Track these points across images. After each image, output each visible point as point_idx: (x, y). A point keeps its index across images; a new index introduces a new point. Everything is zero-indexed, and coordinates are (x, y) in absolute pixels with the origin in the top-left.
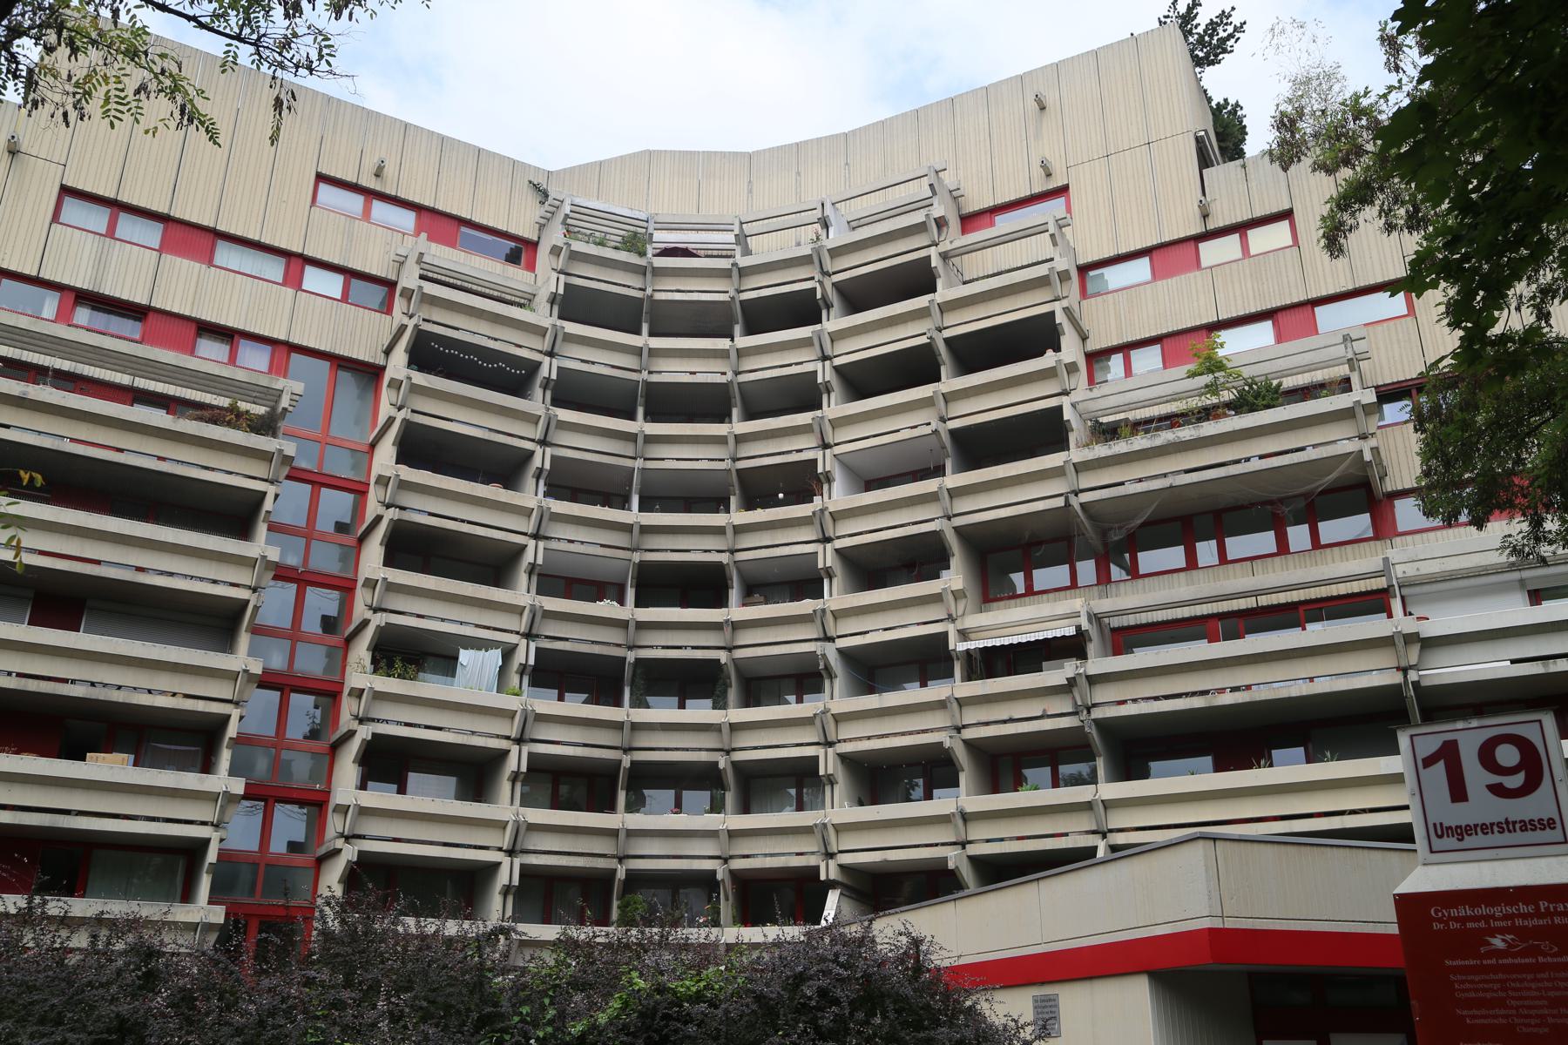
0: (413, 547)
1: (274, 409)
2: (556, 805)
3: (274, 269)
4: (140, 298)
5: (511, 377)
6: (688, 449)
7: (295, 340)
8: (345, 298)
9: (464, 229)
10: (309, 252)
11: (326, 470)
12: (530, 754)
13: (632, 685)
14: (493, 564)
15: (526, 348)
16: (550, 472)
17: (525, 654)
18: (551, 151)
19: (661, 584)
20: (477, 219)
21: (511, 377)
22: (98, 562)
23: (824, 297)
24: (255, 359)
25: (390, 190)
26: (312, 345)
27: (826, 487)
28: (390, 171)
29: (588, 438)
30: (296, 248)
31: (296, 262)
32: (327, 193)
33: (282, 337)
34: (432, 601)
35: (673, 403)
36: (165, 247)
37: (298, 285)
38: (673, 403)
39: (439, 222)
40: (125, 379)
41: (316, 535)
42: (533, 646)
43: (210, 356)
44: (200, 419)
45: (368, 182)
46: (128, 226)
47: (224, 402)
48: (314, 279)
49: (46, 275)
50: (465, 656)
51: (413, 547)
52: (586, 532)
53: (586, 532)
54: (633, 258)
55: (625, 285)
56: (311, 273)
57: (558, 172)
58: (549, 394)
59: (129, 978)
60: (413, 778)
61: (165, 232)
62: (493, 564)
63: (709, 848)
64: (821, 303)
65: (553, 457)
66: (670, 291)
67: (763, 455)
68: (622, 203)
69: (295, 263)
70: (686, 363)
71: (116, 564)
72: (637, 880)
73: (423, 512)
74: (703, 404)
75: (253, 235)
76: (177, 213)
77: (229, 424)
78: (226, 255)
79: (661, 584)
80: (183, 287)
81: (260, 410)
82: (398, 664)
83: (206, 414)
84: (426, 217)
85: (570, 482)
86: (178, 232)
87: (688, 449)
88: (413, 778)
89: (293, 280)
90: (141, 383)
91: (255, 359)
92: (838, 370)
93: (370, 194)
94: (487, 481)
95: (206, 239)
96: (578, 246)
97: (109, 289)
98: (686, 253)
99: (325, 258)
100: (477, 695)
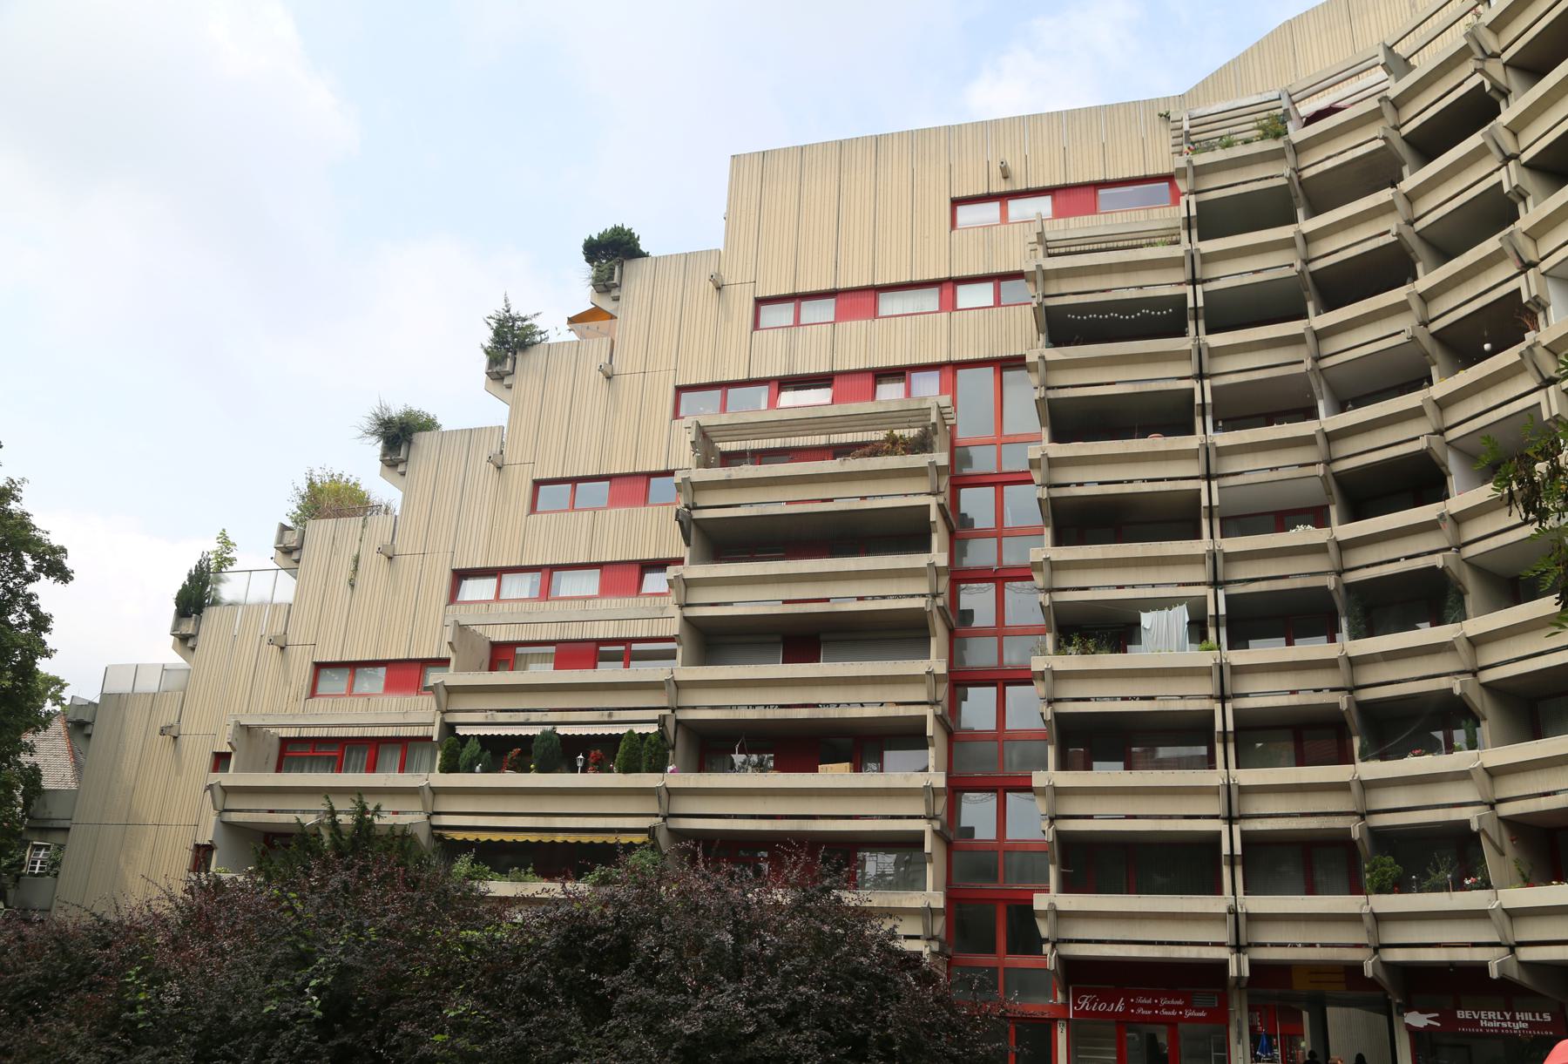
0: (1077, 521)
1: (926, 428)
2: (1301, 762)
3: (929, 300)
4: (824, 368)
5: (1163, 319)
6: (1370, 330)
7: (956, 357)
8: (998, 302)
9: (1101, 192)
10: (956, 274)
11: (1006, 468)
12: (1236, 712)
13: (1348, 615)
14: (1172, 517)
15: (1163, 285)
16: (1214, 405)
17: (1217, 604)
18: (1168, 77)
19: (1368, 492)
20: (1111, 176)
21: (1163, 319)
22: (730, 604)
23: (1493, 87)
24: (927, 388)
25: (1020, 186)
26: (971, 357)
27: (1541, 317)
28: (1016, 168)
29: (1248, 357)
30: (943, 274)
31: (948, 285)
32: (966, 214)
33: (944, 359)
34: (1103, 574)
35: (1341, 285)
36: (841, 316)
37: (953, 307)
38: (1341, 285)
39: (1073, 195)
40: (821, 440)
41: (1005, 532)
42: (1221, 594)
43: (890, 393)
44: (864, 455)
45: (999, 187)
46: (810, 311)
47: (881, 435)
48: (970, 297)
49: (754, 375)
50: (1147, 619)
51: (1077, 521)
52: (1265, 461)
53: (1265, 461)
54: (1271, 145)
55: (1276, 175)
56: (962, 290)
57: (1190, 93)
58: (1201, 324)
59: (29, 931)
60: (889, 756)
61: (941, 293)
62: (1172, 517)
63: (1466, 793)
64: (1494, 95)
65: (1213, 389)
66: (1319, 162)
67: (1457, 306)
68: (1259, 91)
69: (947, 289)
70: (1350, 231)
71: (846, 599)
72: (1382, 838)
73: (1088, 483)
74: (1389, 267)
75: (904, 278)
76: (841, 285)
77: (888, 453)
78: (890, 304)
79: (1368, 492)
80: (861, 344)
81: (913, 433)
82: (1076, 640)
83: (867, 450)
84: (1061, 197)
85: (1238, 409)
86: (846, 301)
87: (1370, 330)
88: (888, 755)
89: (949, 305)
90: (836, 439)
91: (927, 388)
92: (1532, 166)
93: (1003, 197)
94: (1144, 434)
95: (867, 299)
96: (1201, 159)
97: (801, 369)
98: (1331, 111)
99: (971, 273)
100: (1168, 659)
